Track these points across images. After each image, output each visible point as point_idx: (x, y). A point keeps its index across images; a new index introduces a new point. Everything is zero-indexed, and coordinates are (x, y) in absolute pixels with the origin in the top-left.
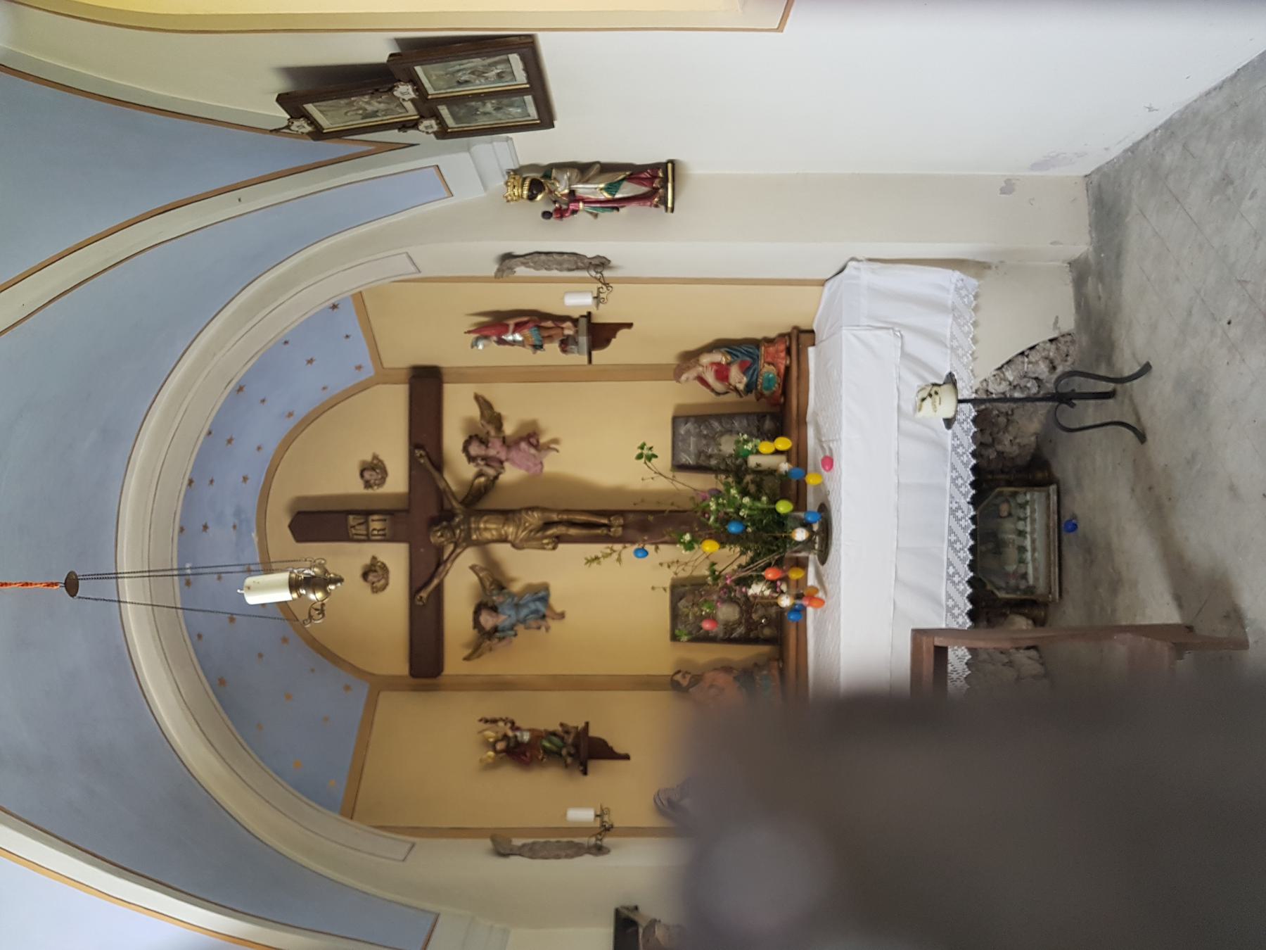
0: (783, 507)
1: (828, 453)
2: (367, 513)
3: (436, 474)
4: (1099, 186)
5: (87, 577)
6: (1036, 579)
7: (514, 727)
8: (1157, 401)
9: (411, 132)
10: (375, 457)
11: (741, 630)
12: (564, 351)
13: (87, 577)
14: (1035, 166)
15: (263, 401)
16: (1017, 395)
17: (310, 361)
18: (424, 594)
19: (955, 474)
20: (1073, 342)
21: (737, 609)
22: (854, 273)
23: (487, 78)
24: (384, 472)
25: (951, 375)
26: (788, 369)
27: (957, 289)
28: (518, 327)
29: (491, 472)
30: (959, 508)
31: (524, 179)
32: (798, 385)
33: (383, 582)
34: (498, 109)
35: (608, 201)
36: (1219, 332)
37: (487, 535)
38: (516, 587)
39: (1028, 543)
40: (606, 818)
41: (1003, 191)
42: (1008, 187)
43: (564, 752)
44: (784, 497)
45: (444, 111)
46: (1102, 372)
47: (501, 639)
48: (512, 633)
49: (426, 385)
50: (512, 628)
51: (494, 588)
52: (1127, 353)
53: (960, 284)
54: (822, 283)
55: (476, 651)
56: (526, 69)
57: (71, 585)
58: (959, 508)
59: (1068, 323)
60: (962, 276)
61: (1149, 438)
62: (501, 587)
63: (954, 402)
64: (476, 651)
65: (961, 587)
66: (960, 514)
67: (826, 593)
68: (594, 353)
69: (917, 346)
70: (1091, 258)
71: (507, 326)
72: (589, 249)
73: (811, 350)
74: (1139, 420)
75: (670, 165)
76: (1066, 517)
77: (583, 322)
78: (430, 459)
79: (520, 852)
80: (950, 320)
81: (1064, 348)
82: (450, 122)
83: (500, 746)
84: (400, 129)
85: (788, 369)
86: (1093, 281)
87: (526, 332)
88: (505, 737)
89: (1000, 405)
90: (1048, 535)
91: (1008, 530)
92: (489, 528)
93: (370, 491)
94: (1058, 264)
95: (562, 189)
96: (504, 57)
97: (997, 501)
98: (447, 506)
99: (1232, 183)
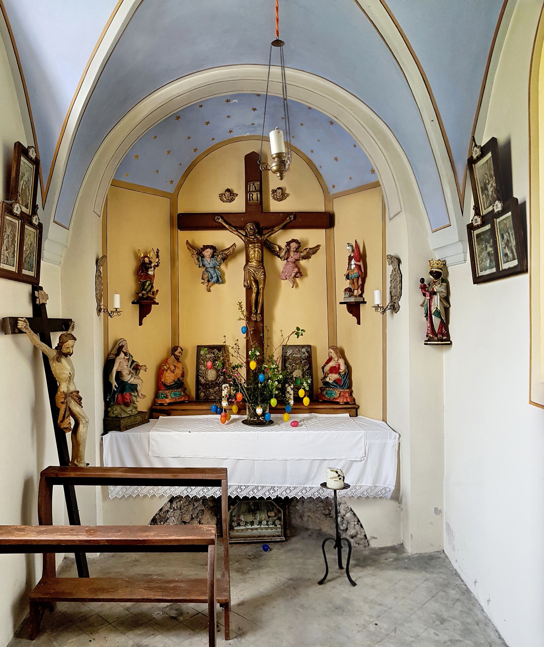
0: (274, 402)
2: (261, 191)
3: (281, 226)
4: (439, 558)
6: (238, 531)
8: (338, 589)
9: (473, 212)
10: (288, 195)
11: (203, 381)
12: (346, 290)
14: (448, 525)
16: (339, 519)
17: (336, 159)
18: (220, 220)
20: (365, 547)
21: (213, 379)
23: (505, 248)
25: (349, 486)
26: (338, 403)
29: (283, 254)
31: (441, 269)
32: (330, 409)
33: (225, 199)
34: (489, 254)
36: (372, 620)
39: (255, 526)
40: (115, 314)
41: (436, 509)
42: (438, 511)
43: (144, 292)
44: (278, 402)
45: (488, 227)
46: (352, 562)
47: (198, 259)
48: (201, 265)
49: (325, 221)
50: (204, 265)
51: (227, 256)
52: (360, 574)
53: (388, 490)
54: (384, 420)
55: (191, 246)
56: (510, 269)
59: (374, 544)
60: (392, 491)
61: (321, 586)
62: (224, 259)
63: (335, 488)
64: (191, 246)
66: (272, 491)
67: (227, 424)
68: (346, 305)
69: (356, 469)
71: (360, 262)
72: (403, 302)
74: (329, 581)
75: (449, 342)
76: (271, 546)
77: (361, 299)
79: (98, 270)
80: (370, 485)
81: (362, 542)
82: (476, 232)
83: (147, 260)
84: (475, 206)
85: (338, 403)
86: (394, 555)
87: (356, 271)
90: (260, 537)
91: (262, 516)
92: (255, 253)
93: (271, 193)
95: (436, 288)
96: (516, 257)
97: (276, 511)
98: (265, 232)
99: (441, 624)
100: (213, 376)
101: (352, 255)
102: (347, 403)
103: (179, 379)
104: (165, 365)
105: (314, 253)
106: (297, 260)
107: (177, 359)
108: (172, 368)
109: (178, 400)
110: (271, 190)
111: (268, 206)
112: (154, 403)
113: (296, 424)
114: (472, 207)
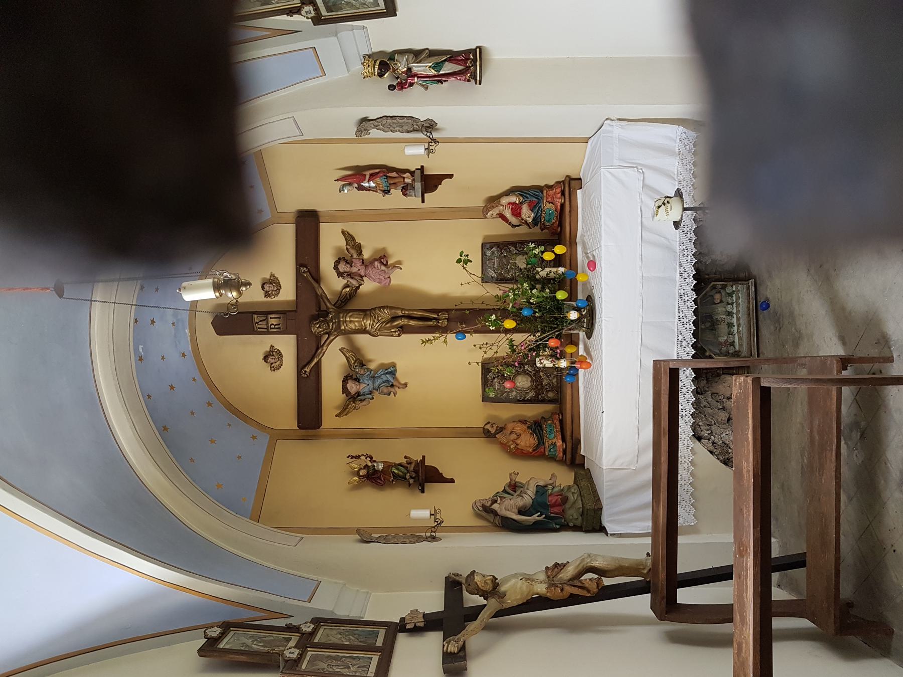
0: (561, 295)
2: (268, 313)
6: (741, 345)
9: (296, 17)
10: (272, 275)
11: (531, 394)
12: (405, 195)
18: (308, 369)
21: (530, 379)
24: (279, 286)
26: (563, 206)
29: (354, 282)
31: (375, 61)
33: (278, 363)
37: (352, 326)
39: (735, 320)
43: (408, 476)
48: (370, 396)
50: (371, 393)
51: (357, 366)
54: (586, 140)
55: (344, 410)
62: (362, 365)
63: (681, 210)
64: (344, 410)
65: (688, 349)
66: (686, 298)
69: (653, 179)
71: (365, 175)
72: (422, 113)
76: (761, 299)
77: (418, 173)
79: (377, 541)
83: (362, 472)
84: (288, 14)
85: (563, 206)
87: (378, 180)
88: (366, 466)
92: (353, 322)
93: (269, 299)
95: (402, 68)
98: (323, 307)
102: (563, 193)
105: (353, 239)
107: (501, 429)
108: (513, 436)
109: (559, 429)
110: (266, 299)
111: (288, 302)
112: (562, 462)
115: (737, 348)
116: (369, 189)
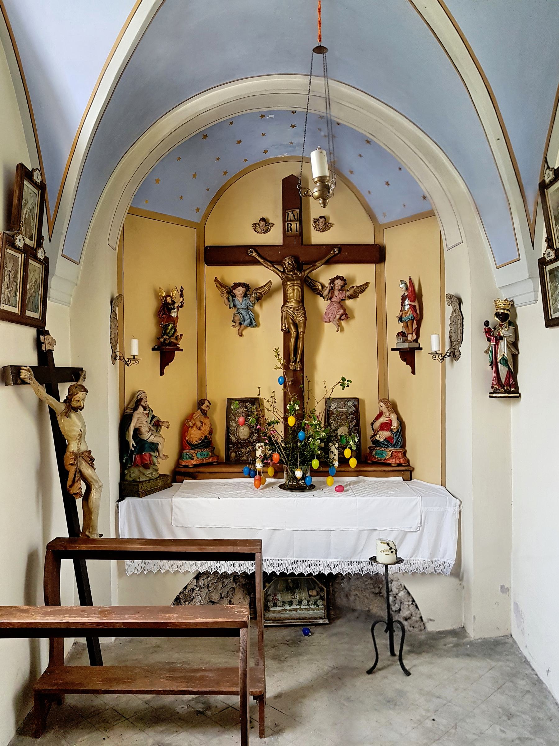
0: (315, 463)
1: (345, 489)
3: (324, 261)
4: (506, 643)
5: (325, 59)
6: (274, 612)
7: (179, 307)
8: (390, 679)
9: (545, 245)
10: (332, 225)
11: (233, 439)
12: (398, 334)
13: (325, 59)
14: (516, 605)
15: (360, 156)
16: (391, 598)
18: (254, 254)
19: (336, 563)
20: (421, 630)
21: (246, 438)
22: (453, 503)
26: (389, 465)
27: (444, 563)
28: (413, 308)
29: (326, 293)
30: (317, 566)
31: (508, 310)
35: (496, 359)
36: (429, 714)
38: (257, 308)
39: (294, 607)
41: (502, 587)
42: (504, 590)
43: (166, 337)
46: (405, 648)
48: (232, 306)
49: (375, 254)
50: (235, 306)
51: (260, 295)
52: (415, 662)
53: (447, 564)
54: (443, 484)
55: (220, 284)
57: (320, 50)
58: (317, 566)
59: (431, 627)
61: (370, 676)
62: (258, 299)
64: (220, 284)
65: (270, 568)
67: (262, 489)
69: (411, 539)
70: (467, 640)
71: (414, 302)
72: (465, 349)
73: (401, 478)
74: (380, 670)
75: (518, 395)
76: (312, 629)
78: (333, 256)
79: (113, 312)
80: (426, 559)
81: (417, 625)
83: (169, 300)
85: (389, 465)
86: (454, 641)
88: (174, 303)
89: (385, 589)
90: (299, 619)
91: (302, 595)
92: (293, 292)
93: (312, 222)
94: (463, 620)
95: (503, 332)
97: (318, 589)
98: (305, 267)
99: (509, 719)
100: (246, 433)
101: (406, 294)
103: (206, 436)
104: (190, 421)
105: (362, 292)
106: (342, 300)
107: (204, 413)
108: (199, 424)
109: (205, 462)
110: (312, 220)
111: (309, 238)
112: (178, 464)
113: (342, 488)
114: (544, 239)
115: (271, 609)
116: (403, 304)
